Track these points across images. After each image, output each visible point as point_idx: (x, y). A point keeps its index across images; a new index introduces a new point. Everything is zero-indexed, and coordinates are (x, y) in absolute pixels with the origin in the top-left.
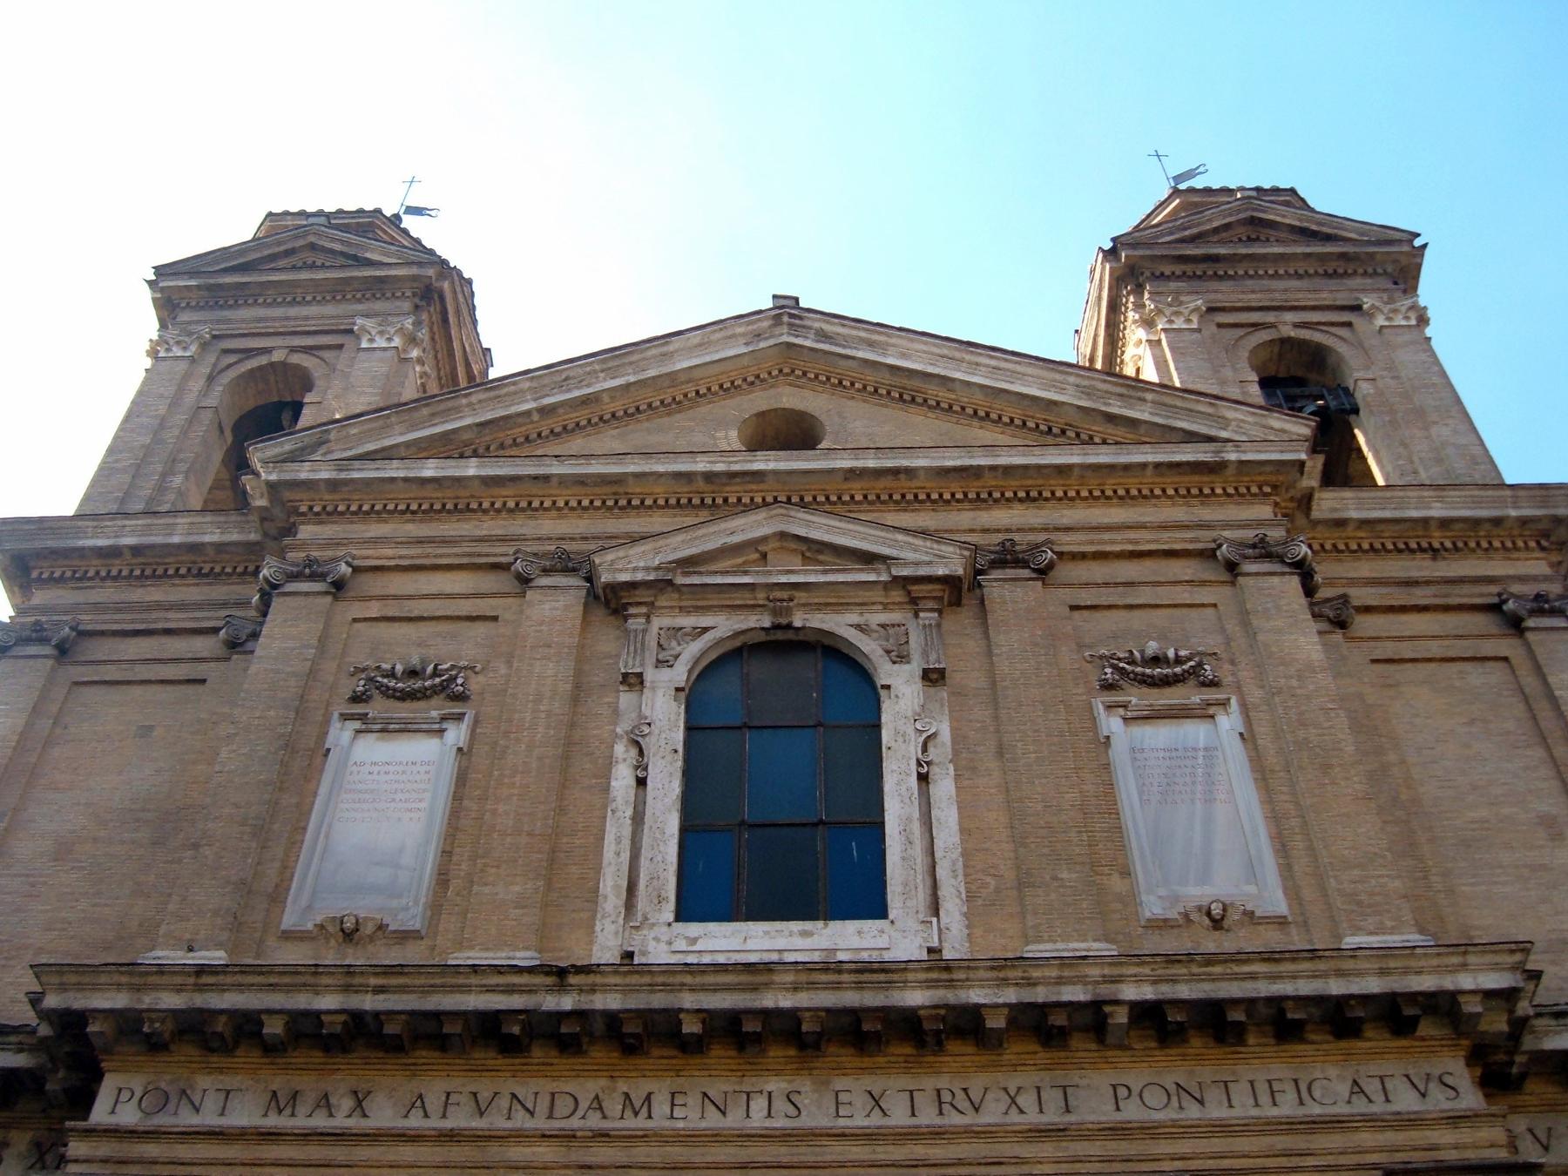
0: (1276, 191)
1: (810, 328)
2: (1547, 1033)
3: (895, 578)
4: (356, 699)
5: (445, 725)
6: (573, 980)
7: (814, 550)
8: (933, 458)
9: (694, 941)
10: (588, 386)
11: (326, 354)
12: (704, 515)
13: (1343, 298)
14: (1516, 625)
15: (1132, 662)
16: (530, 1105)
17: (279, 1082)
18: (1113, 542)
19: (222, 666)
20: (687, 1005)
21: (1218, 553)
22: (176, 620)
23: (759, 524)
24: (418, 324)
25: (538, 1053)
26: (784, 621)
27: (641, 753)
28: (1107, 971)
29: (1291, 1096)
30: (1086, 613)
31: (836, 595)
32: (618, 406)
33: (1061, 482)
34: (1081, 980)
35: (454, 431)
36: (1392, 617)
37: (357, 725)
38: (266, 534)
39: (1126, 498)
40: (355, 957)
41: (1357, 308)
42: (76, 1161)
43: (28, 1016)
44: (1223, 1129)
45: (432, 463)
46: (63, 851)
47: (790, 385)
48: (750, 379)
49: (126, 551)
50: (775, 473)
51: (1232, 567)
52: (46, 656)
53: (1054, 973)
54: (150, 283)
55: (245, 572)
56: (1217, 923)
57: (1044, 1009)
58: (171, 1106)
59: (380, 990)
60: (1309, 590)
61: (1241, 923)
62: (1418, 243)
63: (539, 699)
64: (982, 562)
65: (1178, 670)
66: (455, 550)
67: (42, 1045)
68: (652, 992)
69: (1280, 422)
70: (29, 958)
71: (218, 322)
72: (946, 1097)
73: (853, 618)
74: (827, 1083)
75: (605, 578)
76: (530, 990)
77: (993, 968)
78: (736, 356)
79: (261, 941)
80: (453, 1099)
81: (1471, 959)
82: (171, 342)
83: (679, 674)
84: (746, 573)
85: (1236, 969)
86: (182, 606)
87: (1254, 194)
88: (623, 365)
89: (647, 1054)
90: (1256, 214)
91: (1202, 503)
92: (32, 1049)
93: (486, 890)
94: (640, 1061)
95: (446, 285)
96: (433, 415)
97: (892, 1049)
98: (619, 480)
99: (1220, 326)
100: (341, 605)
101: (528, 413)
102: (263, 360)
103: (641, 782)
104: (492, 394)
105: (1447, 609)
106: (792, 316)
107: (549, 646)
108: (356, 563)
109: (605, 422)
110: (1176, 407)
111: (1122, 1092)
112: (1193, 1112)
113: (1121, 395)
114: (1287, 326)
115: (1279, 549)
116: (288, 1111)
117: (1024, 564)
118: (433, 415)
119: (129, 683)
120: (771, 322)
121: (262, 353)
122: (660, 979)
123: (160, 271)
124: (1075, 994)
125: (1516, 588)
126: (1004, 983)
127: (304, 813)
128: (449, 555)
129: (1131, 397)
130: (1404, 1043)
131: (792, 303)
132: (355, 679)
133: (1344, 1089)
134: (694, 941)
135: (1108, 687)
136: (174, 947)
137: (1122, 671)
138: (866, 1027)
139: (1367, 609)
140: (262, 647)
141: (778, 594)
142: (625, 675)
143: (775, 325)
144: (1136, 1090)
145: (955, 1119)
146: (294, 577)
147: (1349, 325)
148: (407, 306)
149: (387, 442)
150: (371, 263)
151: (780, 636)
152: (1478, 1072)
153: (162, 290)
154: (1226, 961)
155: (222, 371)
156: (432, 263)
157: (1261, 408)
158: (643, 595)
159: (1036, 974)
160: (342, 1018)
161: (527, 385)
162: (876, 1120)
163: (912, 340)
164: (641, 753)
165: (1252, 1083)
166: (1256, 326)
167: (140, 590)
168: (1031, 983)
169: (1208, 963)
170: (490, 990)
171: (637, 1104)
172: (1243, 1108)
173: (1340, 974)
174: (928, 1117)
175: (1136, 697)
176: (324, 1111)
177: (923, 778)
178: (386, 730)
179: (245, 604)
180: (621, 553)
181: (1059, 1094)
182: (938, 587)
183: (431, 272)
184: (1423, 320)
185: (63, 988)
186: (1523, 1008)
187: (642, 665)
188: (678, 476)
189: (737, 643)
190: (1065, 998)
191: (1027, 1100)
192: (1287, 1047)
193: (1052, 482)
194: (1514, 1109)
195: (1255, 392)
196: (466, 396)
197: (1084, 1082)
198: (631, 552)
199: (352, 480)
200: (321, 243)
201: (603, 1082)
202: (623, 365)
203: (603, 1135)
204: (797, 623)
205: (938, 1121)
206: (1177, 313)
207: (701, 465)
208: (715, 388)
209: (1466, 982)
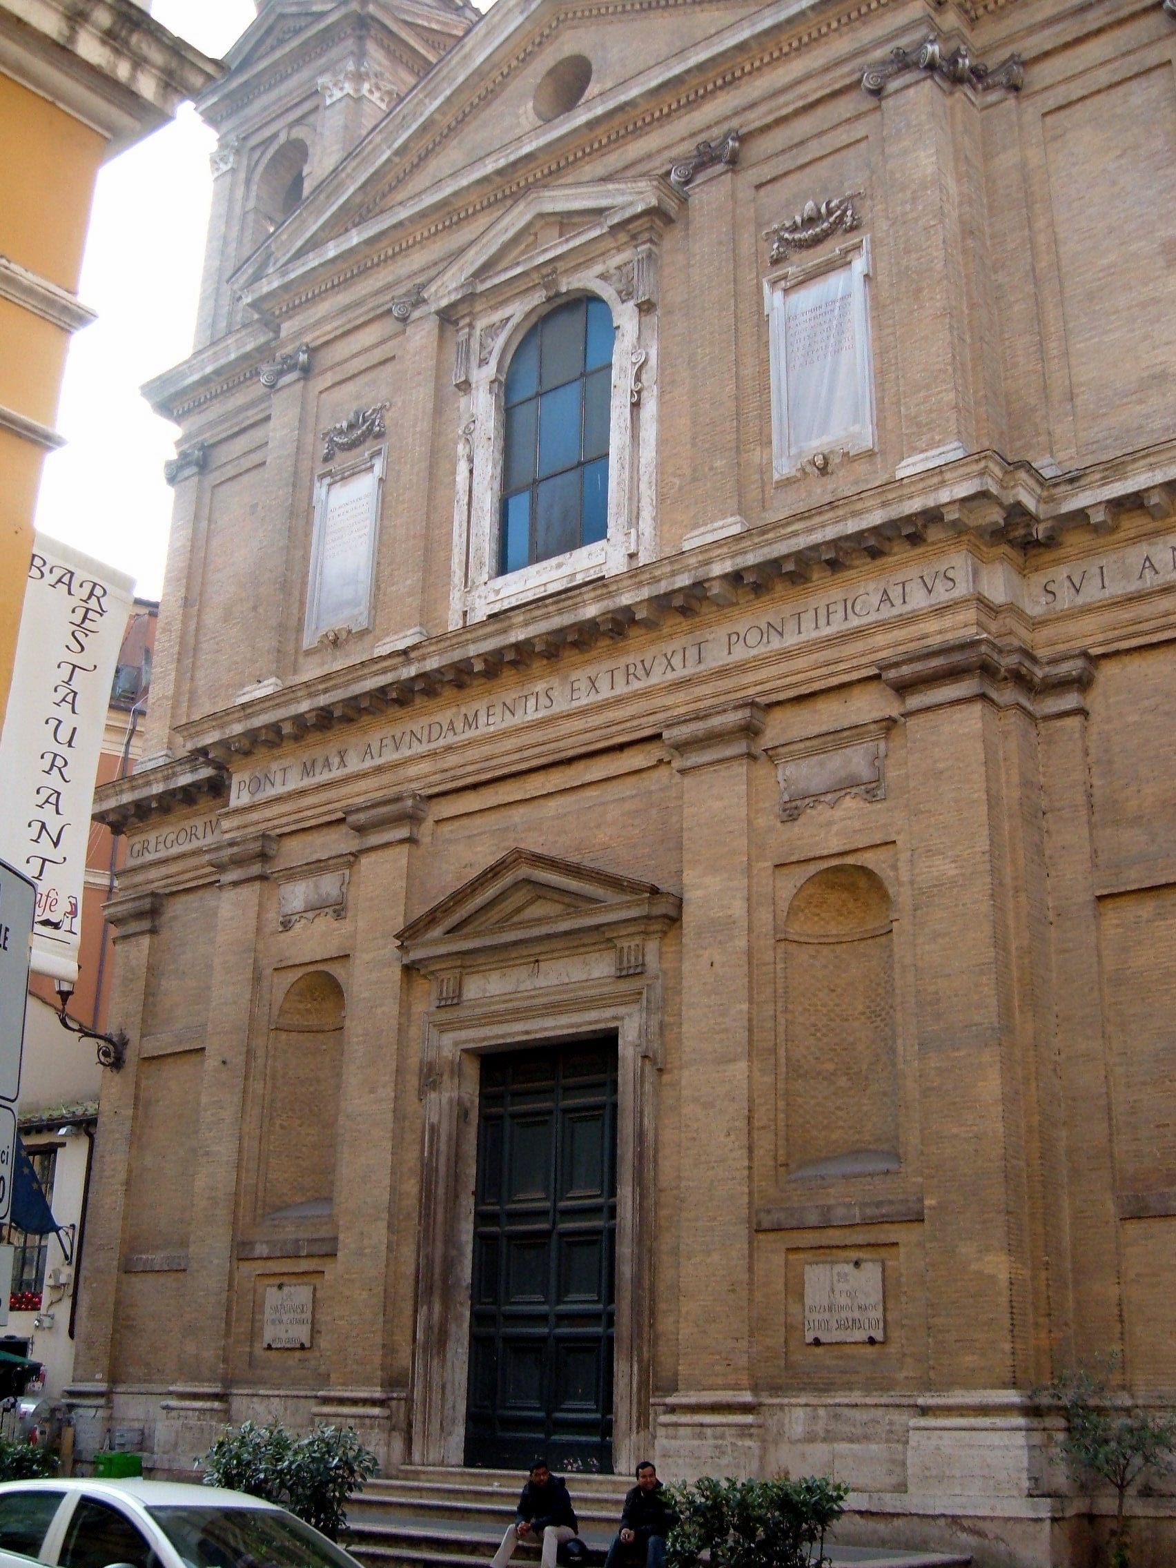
2: (1065, 498)
4: (327, 459)
6: (413, 655)
8: (642, 84)
9: (497, 592)
10: (421, 115)
12: (509, 202)
17: (306, 757)
18: (786, 104)
20: (471, 654)
23: (522, 214)
28: (700, 558)
31: (582, 257)
32: (449, 119)
33: (746, 56)
34: (687, 569)
35: (348, 200)
36: (1070, 53)
37: (328, 480)
39: (802, 48)
45: (331, 244)
48: (537, 40)
49: (213, 376)
50: (540, 149)
53: (668, 569)
57: (669, 595)
59: (326, 691)
61: (842, 464)
66: (364, 309)
72: (632, 670)
74: (566, 677)
76: (395, 668)
77: (631, 577)
78: (516, 30)
79: (296, 661)
80: (385, 742)
81: (948, 476)
84: (518, 264)
85: (783, 531)
89: (470, 686)
91: (864, 23)
93: (394, 588)
94: (466, 692)
96: (328, 197)
97: (599, 644)
98: (444, 203)
100: (311, 383)
101: (389, 160)
103: (471, 471)
104: (358, 160)
105: (1120, 22)
107: (419, 374)
109: (446, 137)
111: (734, 638)
115: (914, 57)
118: (328, 197)
119: (240, 474)
122: (454, 641)
124: (683, 581)
126: (640, 585)
127: (306, 559)
128: (361, 315)
130: (921, 550)
133: (875, 599)
141: (545, 271)
142: (457, 386)
149: (308, 235)
150: (322, 15)
154: (774, 528)
158: (463, 309)
159: (657, 573)
160: (314, 713)
161: (378, 139)
165: (816, 610)
167: (232, 399)
168: (657, 580)
169: (764, 533)
170: (376, 674)
173: (855, 514)
180: (439, 283)
182: (645, 219)
188: (479, 182)
189: (534, 319)
190: (677, 586)
192: (840, 575)
193: (739, 60)
196: (343, 170)
197: (710, 637)
198: (445, 278)
199: (292, 281)
201: (454, 710)
204: (564, 289)
207: (489, 167)
208: (514, 63)
209: (944, 496)
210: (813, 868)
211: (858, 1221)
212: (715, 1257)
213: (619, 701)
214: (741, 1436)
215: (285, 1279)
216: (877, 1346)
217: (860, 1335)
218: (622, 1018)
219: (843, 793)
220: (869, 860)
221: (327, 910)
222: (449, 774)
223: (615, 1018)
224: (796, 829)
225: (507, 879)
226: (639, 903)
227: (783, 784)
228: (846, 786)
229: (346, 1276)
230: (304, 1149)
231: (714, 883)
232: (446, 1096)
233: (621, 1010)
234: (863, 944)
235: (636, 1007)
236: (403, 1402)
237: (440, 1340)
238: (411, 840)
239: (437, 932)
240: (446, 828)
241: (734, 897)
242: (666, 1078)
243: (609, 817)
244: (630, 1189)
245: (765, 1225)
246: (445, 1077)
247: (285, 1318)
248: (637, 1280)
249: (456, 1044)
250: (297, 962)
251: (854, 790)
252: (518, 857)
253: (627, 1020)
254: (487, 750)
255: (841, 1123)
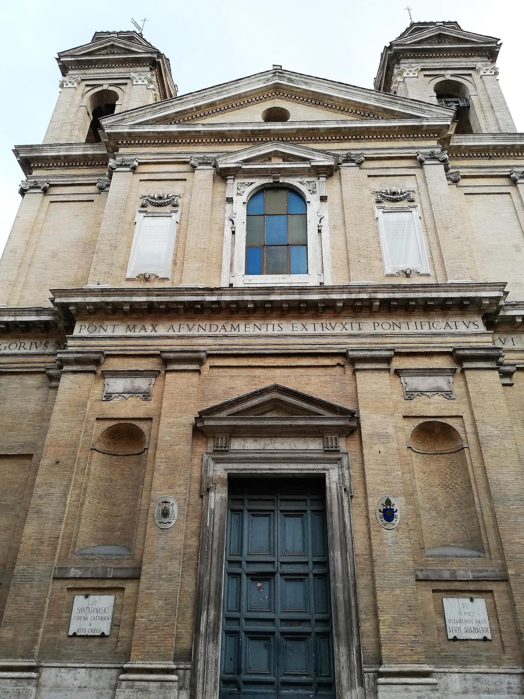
0: (450, 23)
1: (285, 77)
3: (312, 166)
5: (172, 214)
7: (286, 157)
11: (122, 87)
13: (470, 65)
14: (514, 182)
15: (387, 194)
16: (204, 328)
19: (98, 195)
21: (418, 157)
22: (81, 180)
24: (152, 75)
25: (206, 314)
26: (277, 180)
27: (233, 223)
29: (427, 326)
30: (373, 178)
31: (293, 173)
34: (366, 292)
37: (144, 214)
38: (108, 151)
40: (148, 285)
41: (473, 69)
42: (70, 346)
43: (52, 306)
44: (407, 335)
46: (54, 255)
47: (279, 98)
51: (421, 162)
52: (40, 193)
54: (57, 59)
55: (103, 164)
56: (408, 276)
58: (98, 330)
60: (446, 170)
62: (499, 43)
63: (200, 206)
64: (340, 160)
65: (401, 196)
67: (54, 313)
68: (239, 295)
69: (440, 111)
70: (49, 288)
71: (83, 74)
72: (324, 325)
73: (299, 179)
75: (221, 166)
82: (68, 82)
83: (244, 198)
86: (83, 176)
87: (442, 24)
88: (223, 91)
90: (441, 32)
92: (53, 315)
93: (188, 265)
95: (160, 60)
99: (425, 76)
101: (192, 108)
102: (100, 89)
103: (233, 233)
104: (194, 98)
106: (279, 73)
108: (139, 161)
110: (408, 106)
111: (376, 324)
112: (397, 330)
113: (390, 102)
114: (448, 75)
116: (133, 331)
117: (353, 161)
120: (272, 75)
121: (99, 86)
123: (61, 55)
125: (516, 170)
129: (393, 102)
131: (279, 68)
132: (142, 199)
134: (250, 280)
135: (378, 202)
136: (93, 284)
137: (383, 197)
138: (302, 305)
139: (464, 177)
140: (111, 189)
143: (274, 76)
144: (380, 324)
145: (326, 332)
146: (121, 166)
147: (470, 75)
148: (148, 69)
151: (276, 185)
152: (485, 321)
153: (62, 62)
155: (87, 92)
156: (155, 52)
157: (437, 106)
162: (304, 332)
163: (320, 82)
164: (233, 223)
166: (437, 76)
171: (235, 328)
172: (412, 329)
174: (319, 331)
175: (388, 205)
176: (144, 331)
177: (319, 231)
178: (154, 216)
179: (104, 175)
181: (357, 325)
183: (155, 56)
184: (496, 73)
185: (60, 297)
186: (502, 303)
187: (233, 195)
189: (262, 188)
191: (348, 326)
194: (495, 333)
195: (435, 101)
197: (365, 322)
200: (116, 44)
202: (223, 91)
203: (226, 336)
205: (322, 332)
206: (410, 71)
210: (421, 421)
211: (471, 578)
212: (398, 591)
213: (321, 336)
214: (432, 690)
215: (91, 592)
216: (487, 642)
217: (480, 636)
218: (328, 470)
219: (435, 393)
220: (450, 422)
221: (139, 395)
222: (223, 347)
223: (325, 469)
224: (412, 403)
225: (266, 397)
226: (345, 419)
227: (404, 384)
228: (438, 391)
229: (146, 591)
230: (99, 516)
231: (377, 418)
232: (218, 496)
233: (328, 466)
234: (435, 456)
235: (336, 465)
236: (188, 671)
237: (214, 632)
238: (198, 371)
239: (223, 414)
240: (215, 371)
241: (388, 425)
242: (353, 499)
243: (313, 382)
244: (339, 553)
245: (421, 577)
246: (218, 485)
247: (89, 616)
248: (348, 602)
249: (226, 470)
250: (114, 416)
251: (440, 393)
252: (276, 388)
253: (331, 471)
254: (247, 341)
255: (436, 532)
